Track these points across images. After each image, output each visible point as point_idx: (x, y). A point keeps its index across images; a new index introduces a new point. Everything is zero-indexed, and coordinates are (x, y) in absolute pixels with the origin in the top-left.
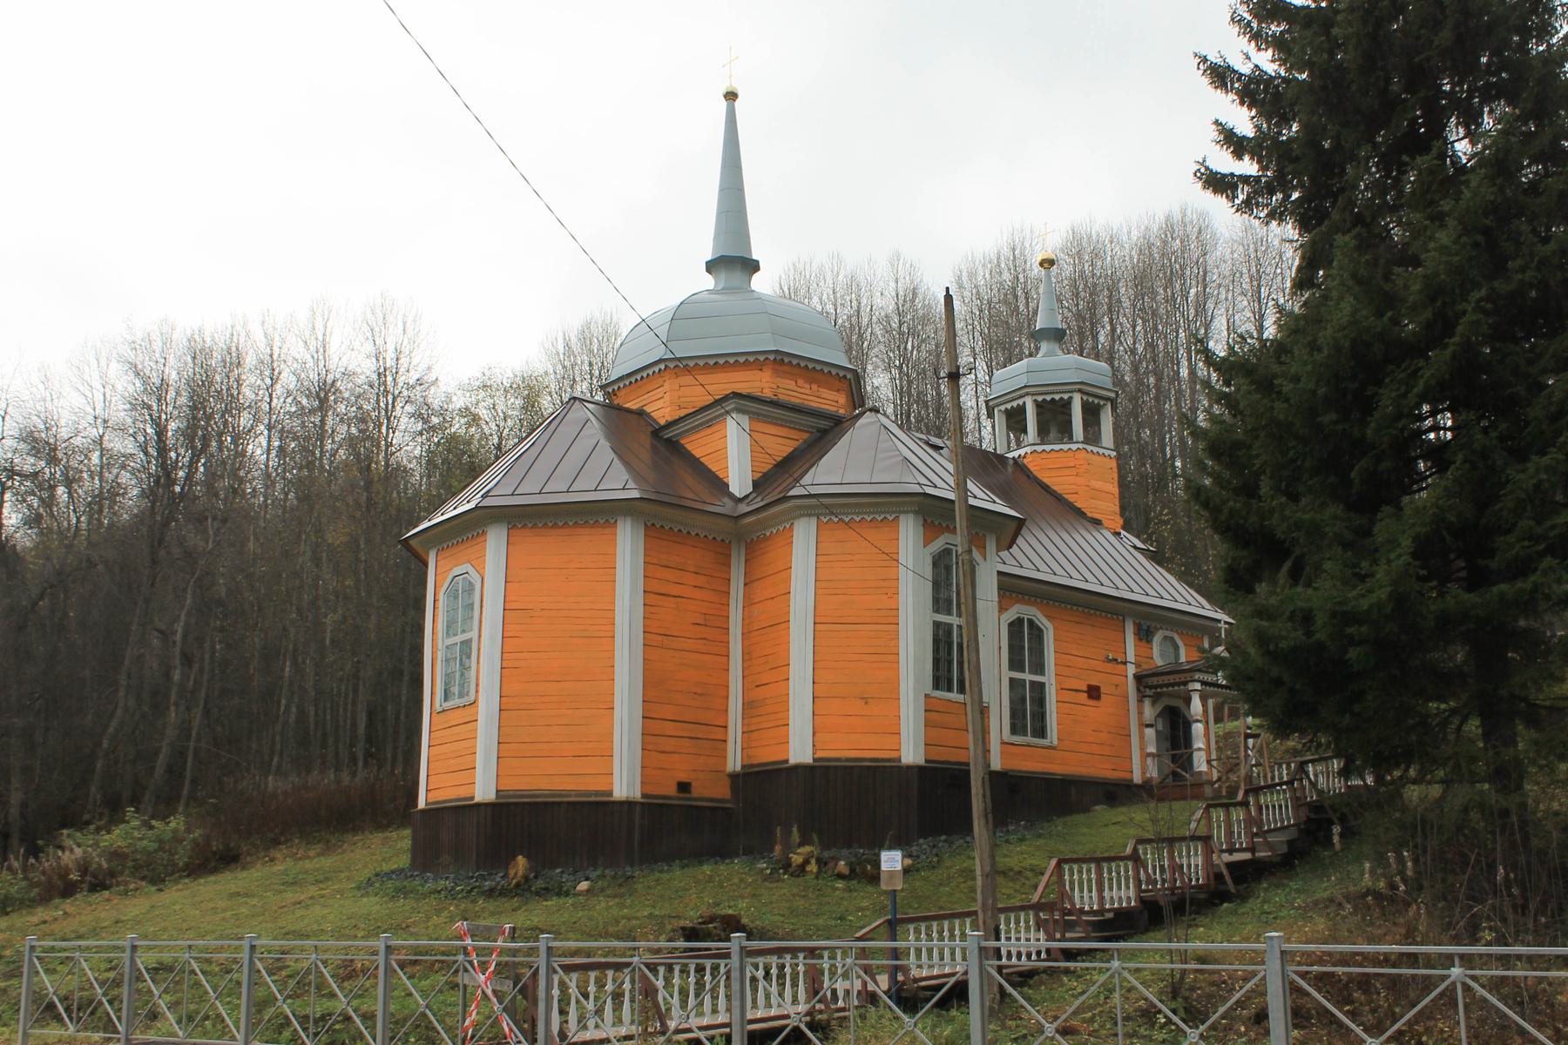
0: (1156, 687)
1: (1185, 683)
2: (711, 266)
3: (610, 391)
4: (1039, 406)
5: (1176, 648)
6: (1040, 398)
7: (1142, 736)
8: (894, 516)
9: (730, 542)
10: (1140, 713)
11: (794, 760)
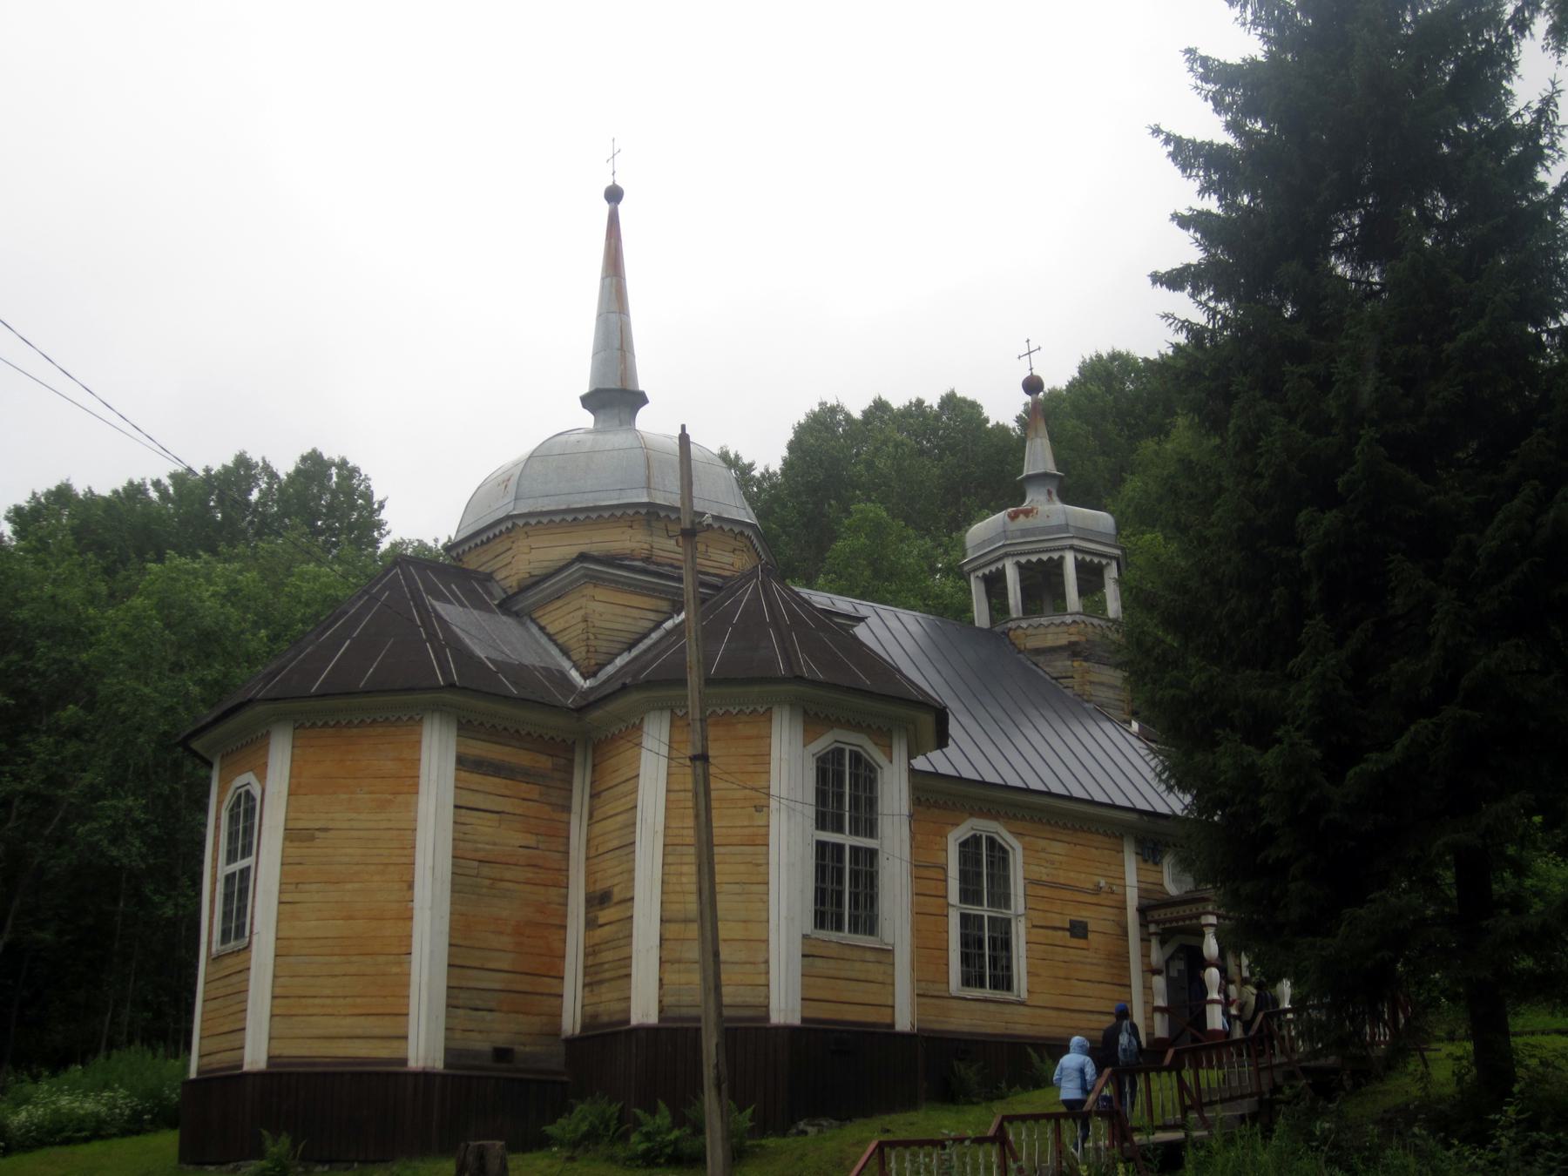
0: (1164, 922)
1: (1198, 916)
2: (588, 401)
3: (455, 555)
6: (1023, 560)
7: (1148, 988)
8: (765, 707)
9: (574, 743)
10: (1146, 955)
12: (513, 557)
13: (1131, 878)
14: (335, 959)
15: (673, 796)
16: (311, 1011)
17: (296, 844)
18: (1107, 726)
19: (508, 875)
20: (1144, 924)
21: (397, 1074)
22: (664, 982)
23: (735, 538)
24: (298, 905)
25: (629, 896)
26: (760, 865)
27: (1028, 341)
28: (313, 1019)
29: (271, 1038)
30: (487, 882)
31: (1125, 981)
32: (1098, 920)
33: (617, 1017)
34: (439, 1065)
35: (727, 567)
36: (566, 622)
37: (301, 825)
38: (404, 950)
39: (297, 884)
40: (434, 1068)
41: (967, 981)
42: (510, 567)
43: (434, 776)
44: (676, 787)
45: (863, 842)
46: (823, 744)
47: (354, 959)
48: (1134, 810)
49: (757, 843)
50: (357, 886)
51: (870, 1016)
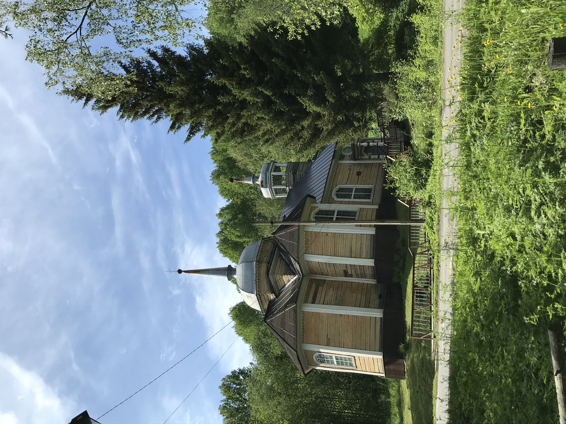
1: (358, 147)
6: (272, 184)
7: (374, 159)
10: (366, 159)
13: (348, 162)
15: (323, 254)
18: (312, 167)
19: (339, 294)
20: (359, 160)
21: (384, 320)
33: (372, 269)
34: (382, 310)
41: (369, 198)
43: (316, 309)
48: (332, 160)
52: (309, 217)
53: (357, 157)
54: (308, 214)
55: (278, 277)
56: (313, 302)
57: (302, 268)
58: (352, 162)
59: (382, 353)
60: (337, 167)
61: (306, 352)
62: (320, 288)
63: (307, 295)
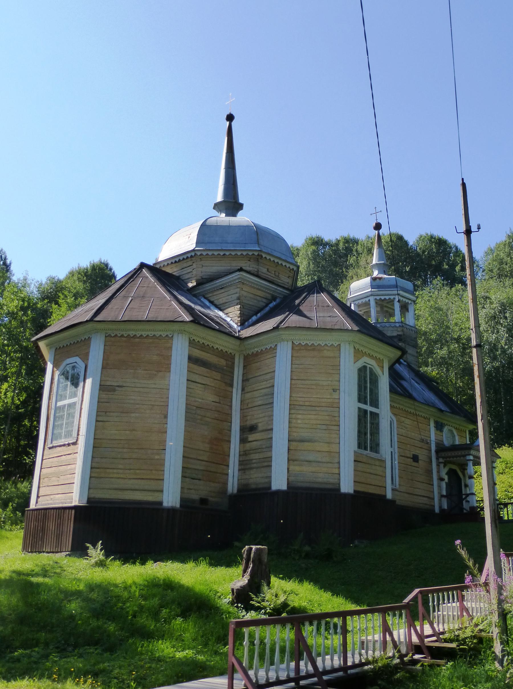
0: (446, 458)
1: (465, 456)
4: (377, 302)
5: (454, 436)
6: (378, 298)
7: (439, 487)
10: (438, 472)
11: (275, 486)
12: (193, 269)
13: (433, 438)
14: (125, 450)
15: (293, 382)
16: (111, 476)
17: (106, 393)
20: (437, 459)
22: (290, 470)
23: (290, 271)
24: (107, 423)
25: (269, 427)
26: (335, 417)
27: (376, 208)
28: (113, 480)
29: (89, 489)
30: (199, 417)
31: (431, 483)
32: (422, 455)
34: (178, 505)
35: (286, 284)
36: (227, 299)
37: (108, 383)
38: (162, 447)
39: (106, 412)
40: (175, 507)
42: (191, 273)
44: (295, 378)
45: (374, 410)
46: (360, 364)
47: (136, 450)
49: (334, 406)
50: (137, 415)
51: (371, 490)
52: (365, 354)
53: (443, 454)
54: (372, 353)
55: (234, 292)
56: (192, 359)
57: (261, 338)
58: (433, 448)
59: (84, 503)
60: (424, 418)
61: (87, 342)
62: (218, 376)
63: (203, 347)
